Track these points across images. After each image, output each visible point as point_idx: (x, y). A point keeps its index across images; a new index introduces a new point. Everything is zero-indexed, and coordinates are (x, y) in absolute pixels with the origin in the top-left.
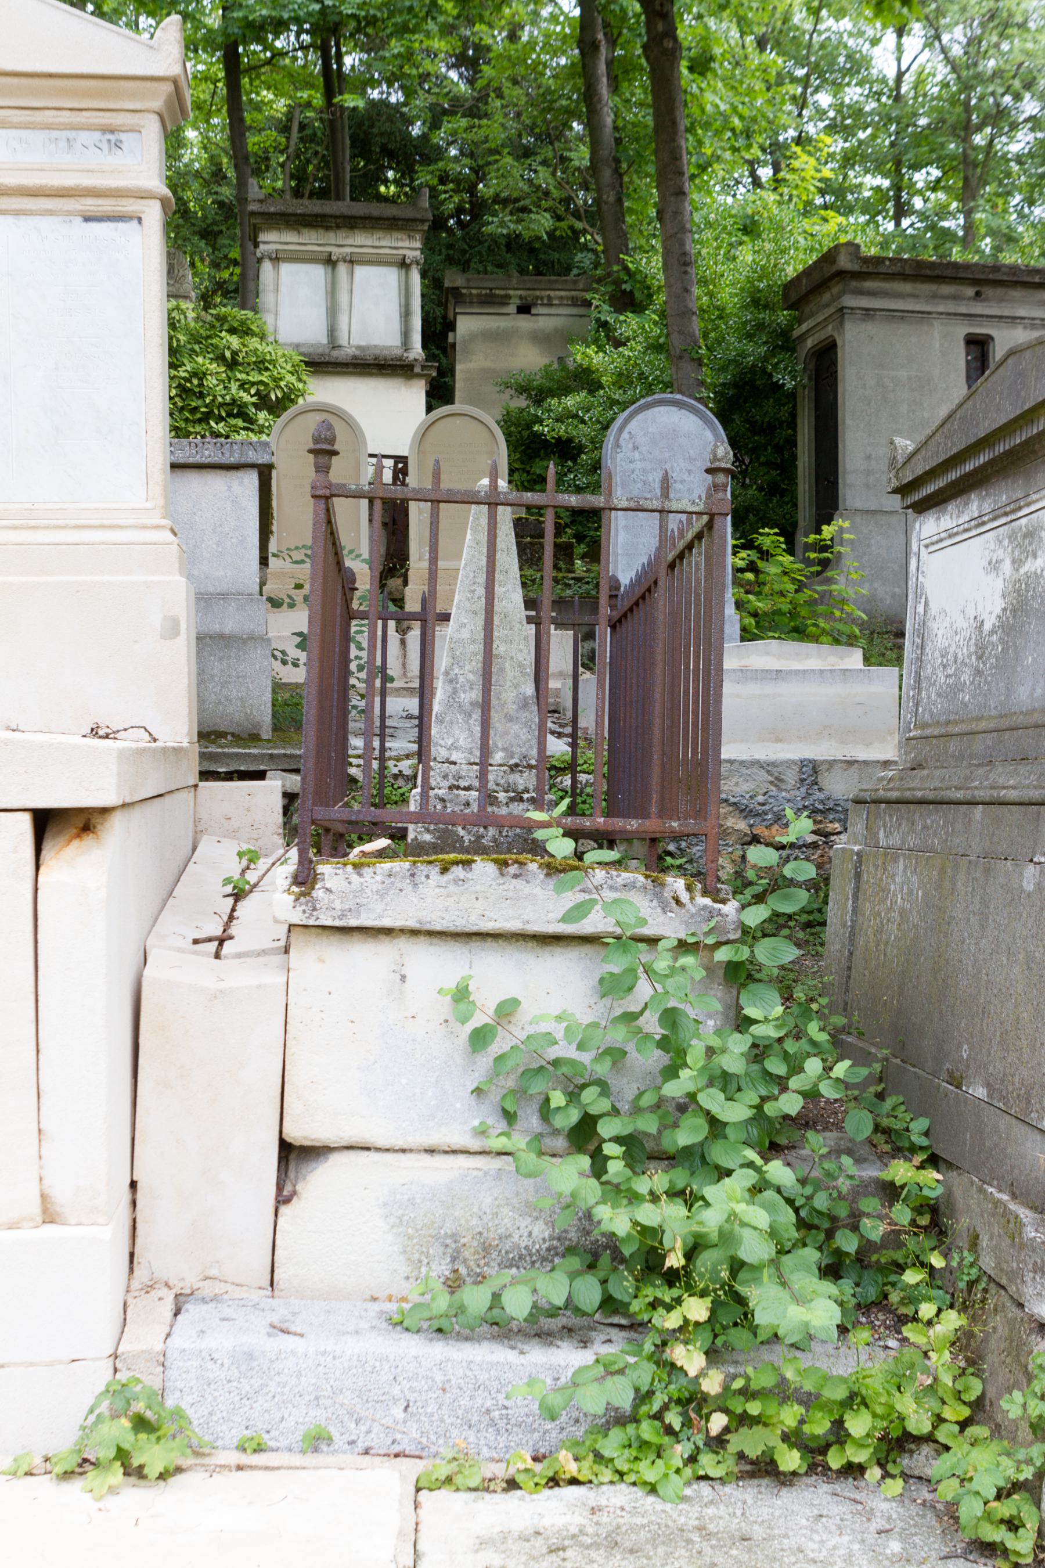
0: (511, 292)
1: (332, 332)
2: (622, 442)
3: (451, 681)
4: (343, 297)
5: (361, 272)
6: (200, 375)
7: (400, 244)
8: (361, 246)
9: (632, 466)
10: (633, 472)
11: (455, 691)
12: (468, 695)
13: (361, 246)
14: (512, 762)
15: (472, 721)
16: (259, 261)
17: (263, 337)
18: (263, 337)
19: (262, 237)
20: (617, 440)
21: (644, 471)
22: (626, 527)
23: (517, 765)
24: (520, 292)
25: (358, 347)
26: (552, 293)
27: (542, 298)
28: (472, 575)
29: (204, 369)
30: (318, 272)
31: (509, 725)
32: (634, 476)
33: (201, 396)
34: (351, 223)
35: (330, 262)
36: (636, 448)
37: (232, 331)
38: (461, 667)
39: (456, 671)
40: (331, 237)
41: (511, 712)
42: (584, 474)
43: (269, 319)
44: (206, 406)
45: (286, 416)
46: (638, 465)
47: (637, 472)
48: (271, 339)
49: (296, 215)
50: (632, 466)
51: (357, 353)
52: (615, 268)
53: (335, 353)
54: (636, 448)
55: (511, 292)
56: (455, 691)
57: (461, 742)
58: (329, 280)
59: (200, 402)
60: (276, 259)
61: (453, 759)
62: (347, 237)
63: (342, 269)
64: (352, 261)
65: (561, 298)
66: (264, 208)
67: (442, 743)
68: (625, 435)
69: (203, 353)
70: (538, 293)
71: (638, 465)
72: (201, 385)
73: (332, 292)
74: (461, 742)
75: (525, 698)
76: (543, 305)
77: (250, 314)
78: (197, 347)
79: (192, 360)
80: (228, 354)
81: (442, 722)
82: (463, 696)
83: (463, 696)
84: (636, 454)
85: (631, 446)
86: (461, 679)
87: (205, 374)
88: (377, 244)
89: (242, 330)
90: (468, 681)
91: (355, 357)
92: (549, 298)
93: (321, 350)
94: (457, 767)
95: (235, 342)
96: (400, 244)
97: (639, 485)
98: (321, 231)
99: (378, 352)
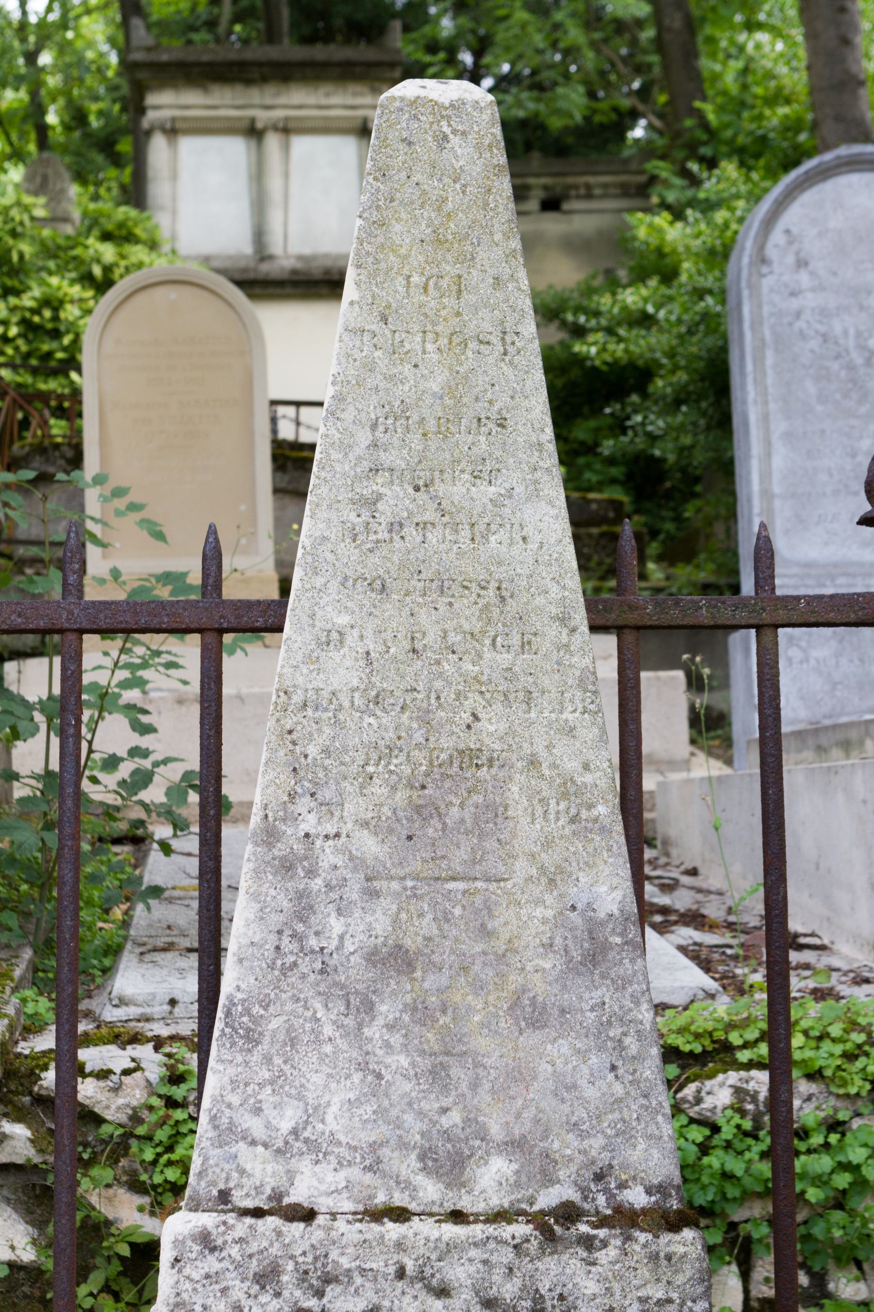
0: (531, 181)
1: (259, 236)
2: (771, 252)
3: (287, 867)
4: (274, 184)
5: (301, 145)
6: (53, 303)
7: (359, 101)
8: (300, 107)
9: (794, 304)
10: (798, 315)
11: (304, 908)
12: (358, 922)
13: (300, 107)
14: (549, 1198)
15: (374, 1031)
16: (149, 133)
17: (153, 245)
18: (153, 245)
19: (152, 99)
20: (761, 247)
21: (824, 313)
22: (788, 436)
23: (568, 1213)
24: (544, 180)
25: (300, 258)
26: (591, 180)
27: (576, 187)
28: (364, 437)
29: (60, 294)
30: (236, 148)
31: (531, 1039)
32: (800, 324)
33: (56, 334)
34: (284, 73)
35: (253, 132)
36: (801, 263)
37: (106, 237)
38: (327, 808)
39: (309, 823)
40: (255, 95)
41: (539, 987)
42: (659, 414)
43: (162, 221)
44: (65, 349)
45: (112, 295)
46: (810, 300)
47: (807, 315)
48: (166, 248)
49: (199, 64)
50: (794, 304)
51: (299, 265)
52: (689, 123)
53: (265, 268)
54: (801, 263)
55: (531, 181)
56: (304, 908)
57: (334, 1122)
58: (254, 158)
59: (54, 345)
60: (173, 131)
61: (298, 1195)
62: (277, 95)
63: (272, 141)
64: (286, 130)
65: (605, 186)
66: (152, 57)
67: (255, 1126)
68: (777, 237)
69: (60, 271)
70: (570, 180)
71: (810, 300)
72: (56, 318)
73: (258, 176)
74: (334, 1122)
75: (593, 927)
76: (579, 197)
77: (133, 213)
78: (52, 264)
79: (43, 283)
80: (97, 271)
81: (252, 1038)
82: (336, 925)
83: (336, 925)
84: (804, 279)
85: (790, 259)
86: (328, 856)
87: (61, 302)
88: (324, 101)
89: (120, 236)
90: (356, 862)
91: (294, 272)
92: (588, 187)
93: (242, 264)
94: (316, 1233)
95: (108, 252)
96: (359, 101)
97: (814, 344)
98: (239, 88)
99: (329, 263)
